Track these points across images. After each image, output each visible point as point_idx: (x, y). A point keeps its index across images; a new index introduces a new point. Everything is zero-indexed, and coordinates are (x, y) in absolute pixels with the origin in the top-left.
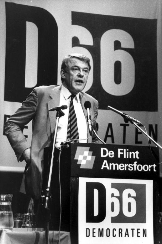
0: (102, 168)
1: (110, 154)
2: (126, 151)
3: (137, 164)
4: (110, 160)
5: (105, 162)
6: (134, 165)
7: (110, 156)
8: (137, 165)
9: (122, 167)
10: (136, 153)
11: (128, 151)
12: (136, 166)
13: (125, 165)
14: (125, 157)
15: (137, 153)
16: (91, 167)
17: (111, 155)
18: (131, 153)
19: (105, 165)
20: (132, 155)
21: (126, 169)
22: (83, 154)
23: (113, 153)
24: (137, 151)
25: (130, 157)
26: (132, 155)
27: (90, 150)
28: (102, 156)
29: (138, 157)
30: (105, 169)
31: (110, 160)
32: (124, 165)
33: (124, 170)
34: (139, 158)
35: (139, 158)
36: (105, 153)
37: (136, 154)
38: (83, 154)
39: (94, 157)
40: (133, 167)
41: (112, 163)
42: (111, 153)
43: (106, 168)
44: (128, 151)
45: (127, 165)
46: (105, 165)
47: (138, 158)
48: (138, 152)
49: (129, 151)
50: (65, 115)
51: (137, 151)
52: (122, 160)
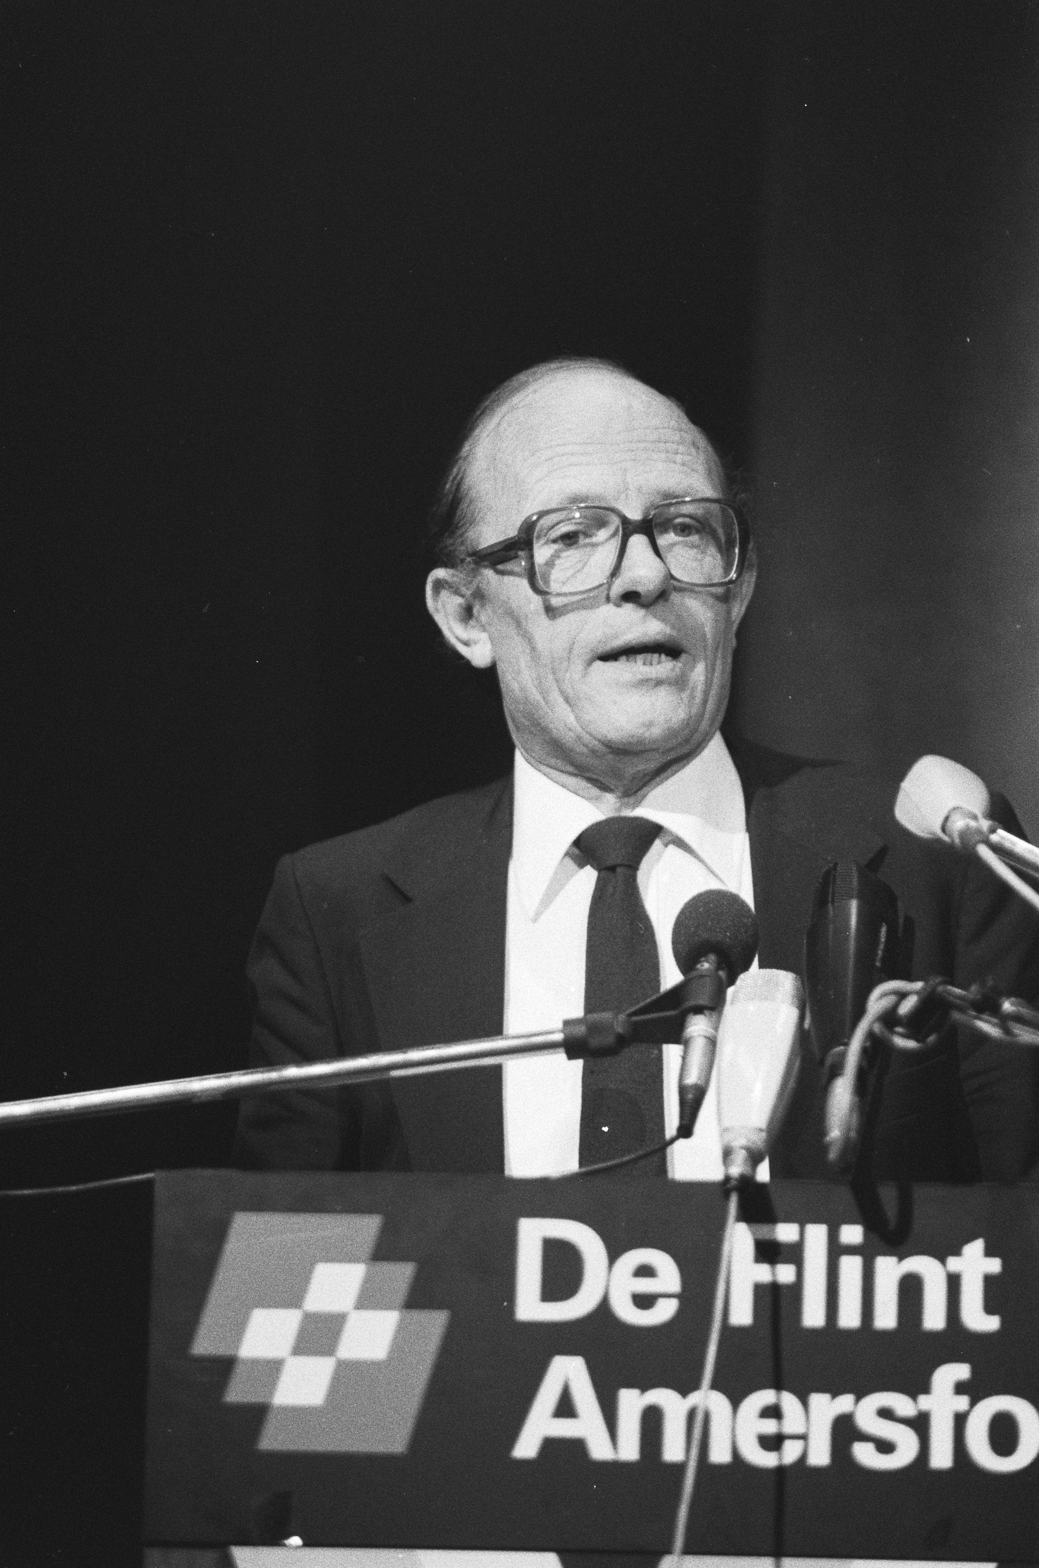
0: (527, 1447)
1: (630, 1283)
2: (836, 1250)
3: (973, 1390)
4: (619, 1355)
5: (568, 1371)
6: (925, 1402)
7: (627, 1313)
8: (962, 1403)
9: (645, 1286)
10: (954, 1264)
11: (851, 1250)
12: (960, 1420)
13: (819, 1401)
14: (813, 1316)
15: (975, 1263)
16: (388, 1431)
17: (644, 1301)
18: (889, 1271)
19: (565, 1411)
20: (911, 1290)
21: (820, 1455)
22: (293, 1299)
23: (668, 1276)
24: (975, 1248)
25: (886, 1318)
26: (911, 1290)
27: (383, 1252)
28: (530, 1306)
29: (989, 1308)
30: (564, 1452)
31: (619, 1355)
32: (805, 1404)
33: (804, 1457)
34: (991, 1324)
35: (991, 1324)
36: (562, 1271)
37: (954, 1282)
38: (293, 1299)
39: (435, 1323)
40: (920, 1424)
41: (644, 1388)
42: (645, 1271)
43: (577, 1446)
44: (851, 1250)
45: (845, 1403)
46: (565, 1408)
47: (979, 1320)
48: (989, 1252)
49: (867, 1253)
50: (896, 1453)
51: (975, 1248)
52: (779, 1353)
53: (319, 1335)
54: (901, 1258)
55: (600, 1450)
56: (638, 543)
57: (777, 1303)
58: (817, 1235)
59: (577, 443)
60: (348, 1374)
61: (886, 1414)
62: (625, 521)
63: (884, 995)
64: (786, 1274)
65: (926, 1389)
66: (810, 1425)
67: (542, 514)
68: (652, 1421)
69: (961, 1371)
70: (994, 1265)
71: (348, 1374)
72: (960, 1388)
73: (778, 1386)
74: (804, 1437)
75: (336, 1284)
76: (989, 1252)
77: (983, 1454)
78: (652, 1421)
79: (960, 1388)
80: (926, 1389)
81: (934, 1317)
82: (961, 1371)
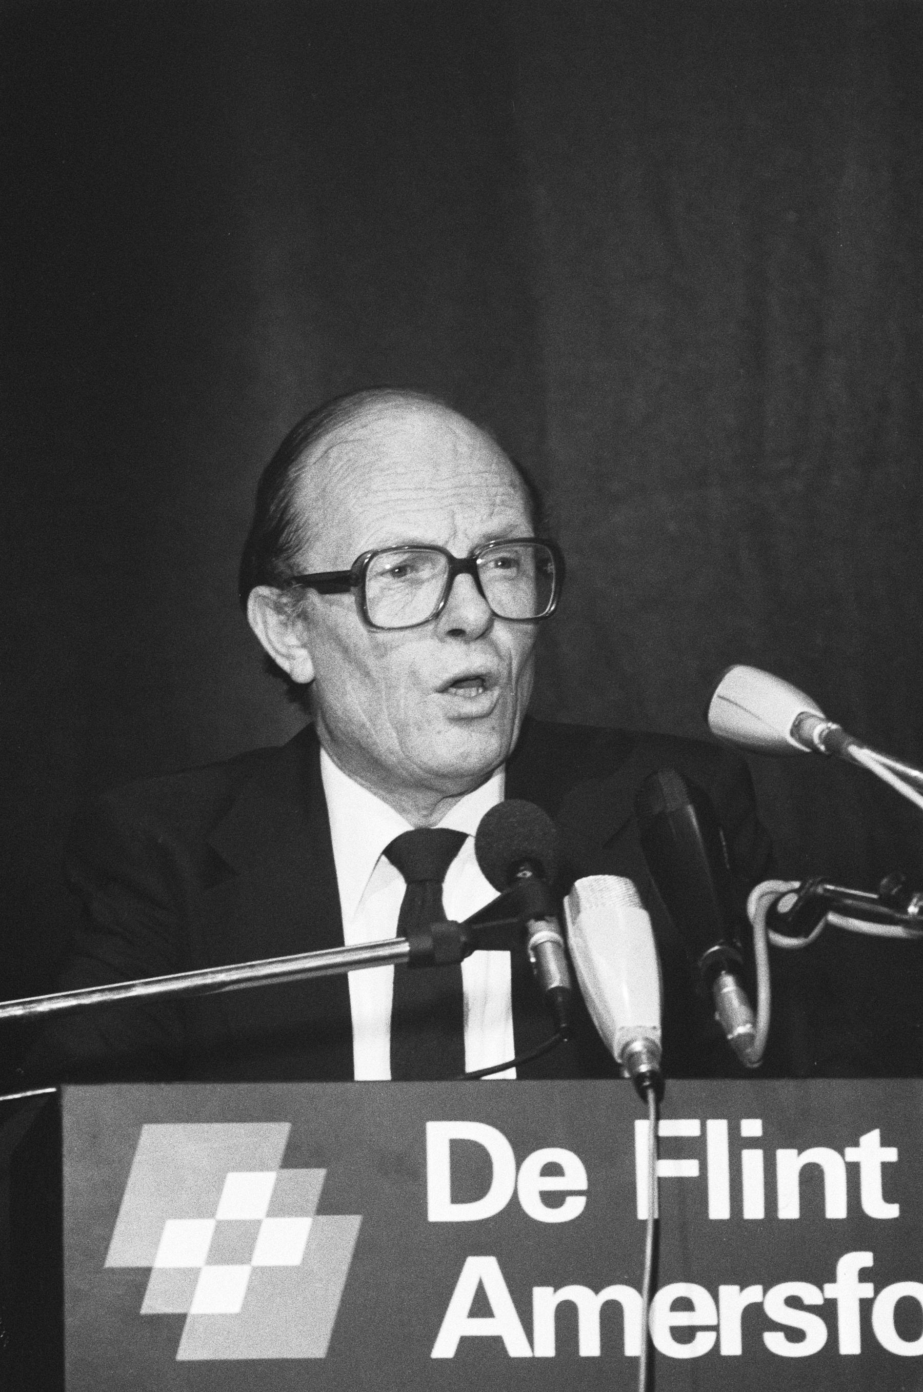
0: (444, 1348)
2: (737, 1144)
4: (531, 1254)
5: (482, 1271)
6: (830, 1290)
8: (867, 1290)
9: (553, 1184)
10: (852, 1154)
11: (752, 1143)
12: (866, 1306)
13: (728, 1292)
14: (719, 1208)
15: (873, 1153)
17: (553, 1199)
18: (790, 1163)
19: (483, 1307)
20: (812, 1179)
21: (732, 1346)
22: (205, 1210)
23: (575, 1175)
24: (872, 1139)
25: (789, 1208)
26: (812, 1179)
28: (441, 1207)
29: (888, 1197)
30: (481, 1351)
31: (531, 1254)
34: (892, 1211)
35: (892, 1211)
36: (471, 1172)
37: (853, 1170)
40: (828, 1312)
42: (552, 1170)
44: (752, 1143)
45: (754, 1293)
46: (481, 1307)
47: (878, 1207)
48: (885, 1143)
49: (768, 1145)
50: (801, 1344)
51: (872, 1139)
52: (690, 1244)
53: (233, 1244)
54: (801, 1150)
55: (517, 1347)
56: (463, 581)
57: (683, 1196)
58: (718, 1129)
59: (403, 480)
60: (267, 1282)
61: (794, 1302)
62: (451, 559)
63: (762, 896)
64: (688, 1168)
65: (832, 1279)
66: (718, 1317)
67: (375, 554)
68: (567, 1316)
69: (865, 1259)
70: (891, 1155)
71: (267, 1282)
72: (864, 1275)
73: (688, 1278)
74: (716, 1328)
75: (249, 1191)
76: (885, 1143)
77: (890, 1340)
78: (567, 1316)
79: (864, 1275)
80: (832, 1278)
81: (836, 1207)
82: (865, 1259)
